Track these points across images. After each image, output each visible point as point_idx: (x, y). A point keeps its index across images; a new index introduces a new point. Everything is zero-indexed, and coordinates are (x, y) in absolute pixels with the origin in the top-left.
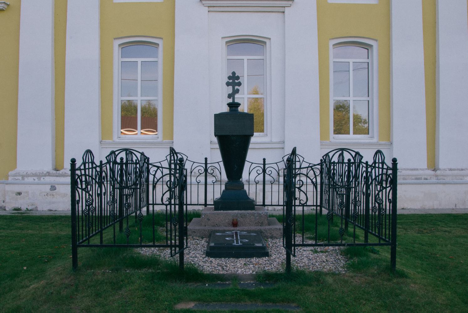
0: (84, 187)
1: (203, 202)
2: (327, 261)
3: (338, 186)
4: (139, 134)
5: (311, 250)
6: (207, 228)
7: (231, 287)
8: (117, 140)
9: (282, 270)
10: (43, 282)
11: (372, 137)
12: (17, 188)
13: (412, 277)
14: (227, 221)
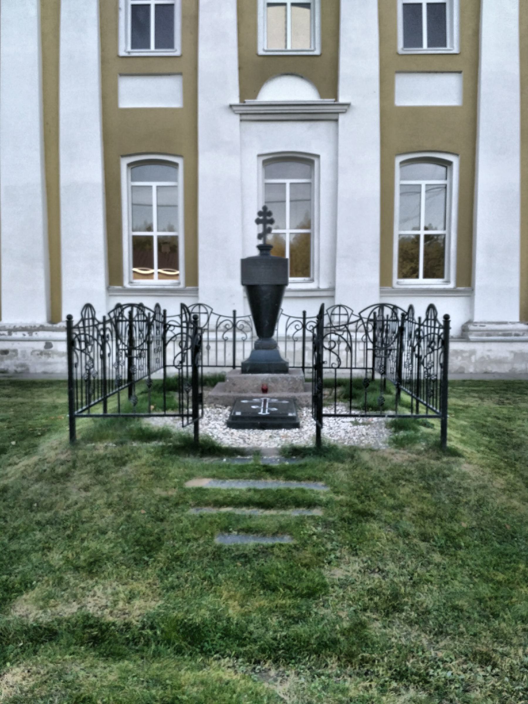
0: (83, 347)
1: (231, 364)
2: (367, 434)
4: (156, 276)
5: (352, 422)
6: (232, 394)
7: (252, 462)
9: (311, 444)
10: (35, 459)
11: (448, 282)
13: (468, 455)
14: (255, 386)
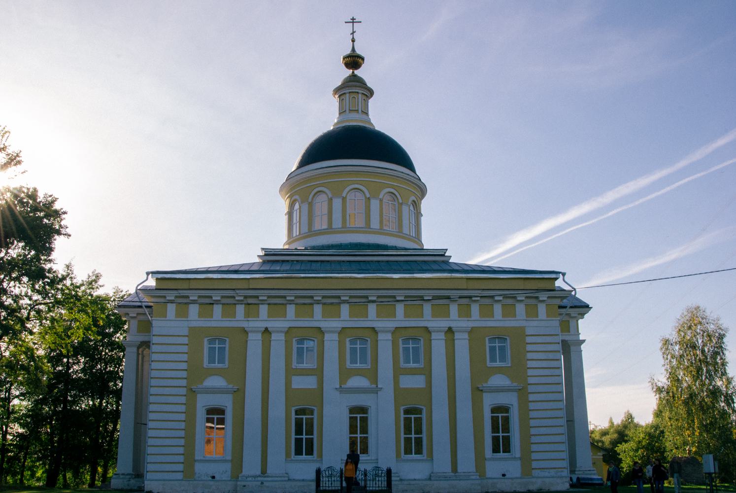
3: (81, 397)
8: (293, 459)
12: (243, 483)
